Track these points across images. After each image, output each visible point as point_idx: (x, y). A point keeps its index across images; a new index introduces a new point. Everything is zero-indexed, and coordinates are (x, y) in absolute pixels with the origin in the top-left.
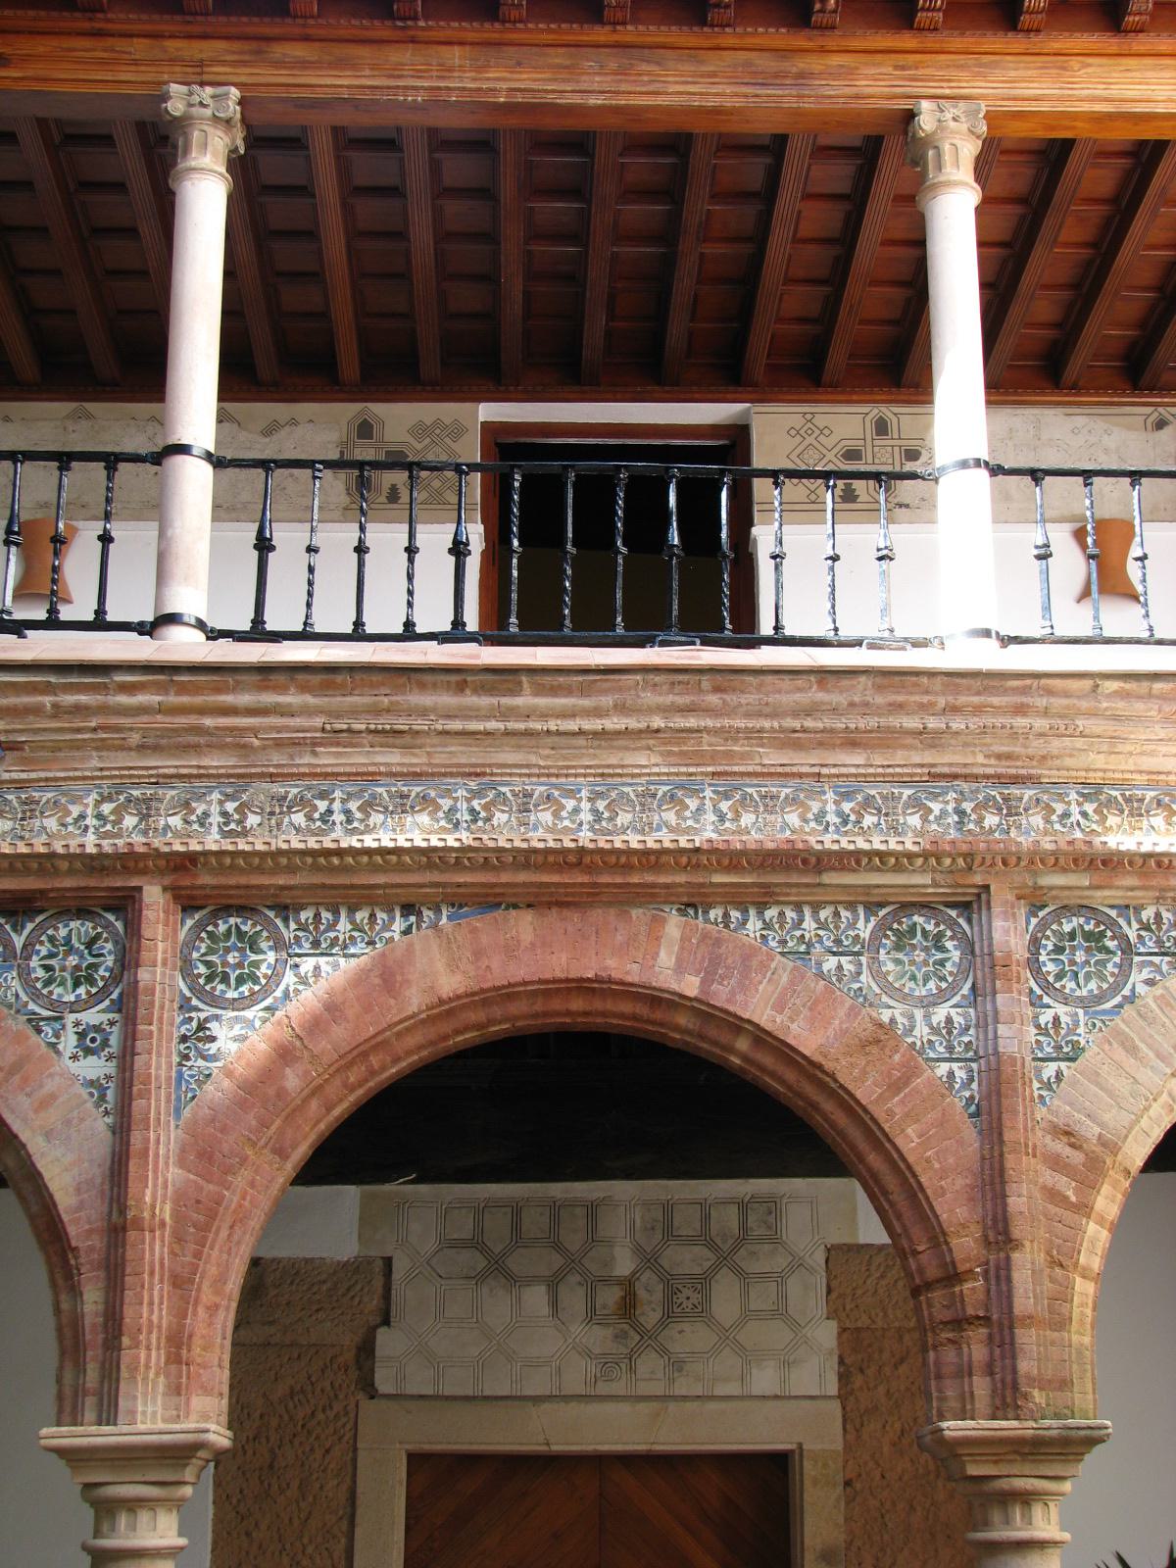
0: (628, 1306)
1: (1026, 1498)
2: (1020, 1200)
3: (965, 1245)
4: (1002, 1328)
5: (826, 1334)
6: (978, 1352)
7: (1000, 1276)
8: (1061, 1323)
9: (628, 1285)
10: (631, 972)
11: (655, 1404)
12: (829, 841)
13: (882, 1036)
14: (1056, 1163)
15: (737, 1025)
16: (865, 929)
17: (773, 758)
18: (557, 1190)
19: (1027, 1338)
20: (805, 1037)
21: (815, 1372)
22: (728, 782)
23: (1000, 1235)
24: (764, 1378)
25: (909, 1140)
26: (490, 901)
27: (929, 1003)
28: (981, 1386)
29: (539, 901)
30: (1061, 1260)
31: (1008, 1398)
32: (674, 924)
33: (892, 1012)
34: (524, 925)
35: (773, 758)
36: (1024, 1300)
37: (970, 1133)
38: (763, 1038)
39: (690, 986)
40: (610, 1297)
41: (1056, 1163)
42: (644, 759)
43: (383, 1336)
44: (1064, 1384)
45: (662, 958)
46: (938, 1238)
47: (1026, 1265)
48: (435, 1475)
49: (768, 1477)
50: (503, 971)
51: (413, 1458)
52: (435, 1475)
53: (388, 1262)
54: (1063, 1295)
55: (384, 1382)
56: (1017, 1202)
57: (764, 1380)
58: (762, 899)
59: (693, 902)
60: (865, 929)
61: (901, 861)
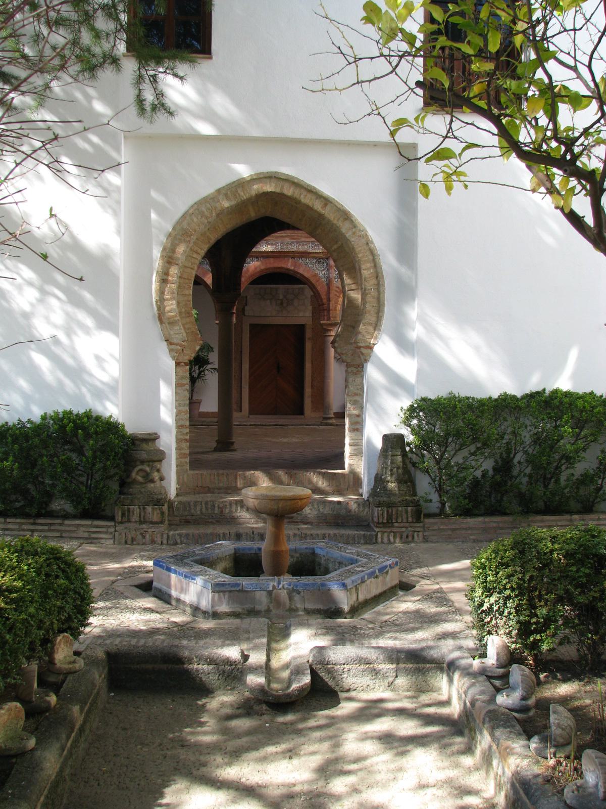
0: (282, 304)
1: (330, 330)
2: (332, 296)
3: (325, 301)
4: (328, 310)
5: (310, 308)
6: (325, 313)
7: (329, 305)
8: (336, 310)
9: (282, 300)
10: (284, 266)
11: (595, 43)
12: (311, 250)
13: (316, 275)
14: (337, 291)
15: (298, 273)
16: (314, 261)
17: (303, 239)
18: (272, 286)
19: (331, 312)
20: (306, 275)
21: (308, 314)
22: (298, 242)
23: (329, 300)
24: (302, 315)
25: (319, 288)
26: (268, 257)
27: (322, 271)
28: (326, 318)
29: (273, 257)
30: (336, 303)
31: (328, 319)
32: (291, 260)
33: (317, 272)
34: (272, 260)
35: (303, 239)
36: (331, 307)
37: (326, 287)
38: (301, 275)
39: (292, 268)
40: (279, 302)
41: (337, 291)
42: (288, 239)
43: (246, 307)
44: (335, 317)
45: (289, 265)
46: (322, 300)
47: (332, 303)
48: (253, 327)
49: (301, 328)
50: (269, 266)
51: (251, 325)
52: (253, 327)
53: (246, 297)
54: (336, 307)
55: (246, 313)
56: (331, 296)
57: (301, 314)
58: (301, 257)
59: (293, 258)
60: (314, 261)
61: (319, 253)
